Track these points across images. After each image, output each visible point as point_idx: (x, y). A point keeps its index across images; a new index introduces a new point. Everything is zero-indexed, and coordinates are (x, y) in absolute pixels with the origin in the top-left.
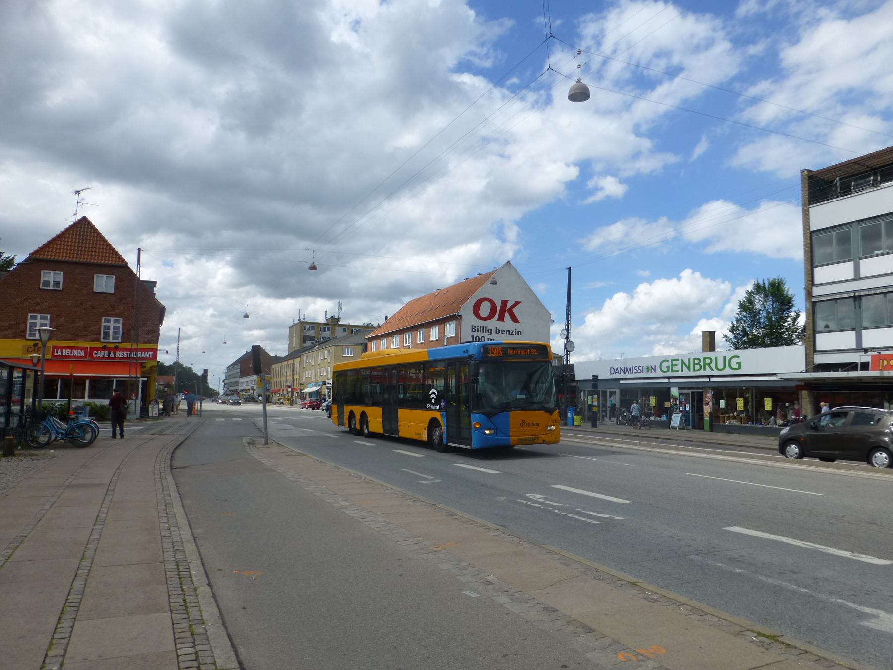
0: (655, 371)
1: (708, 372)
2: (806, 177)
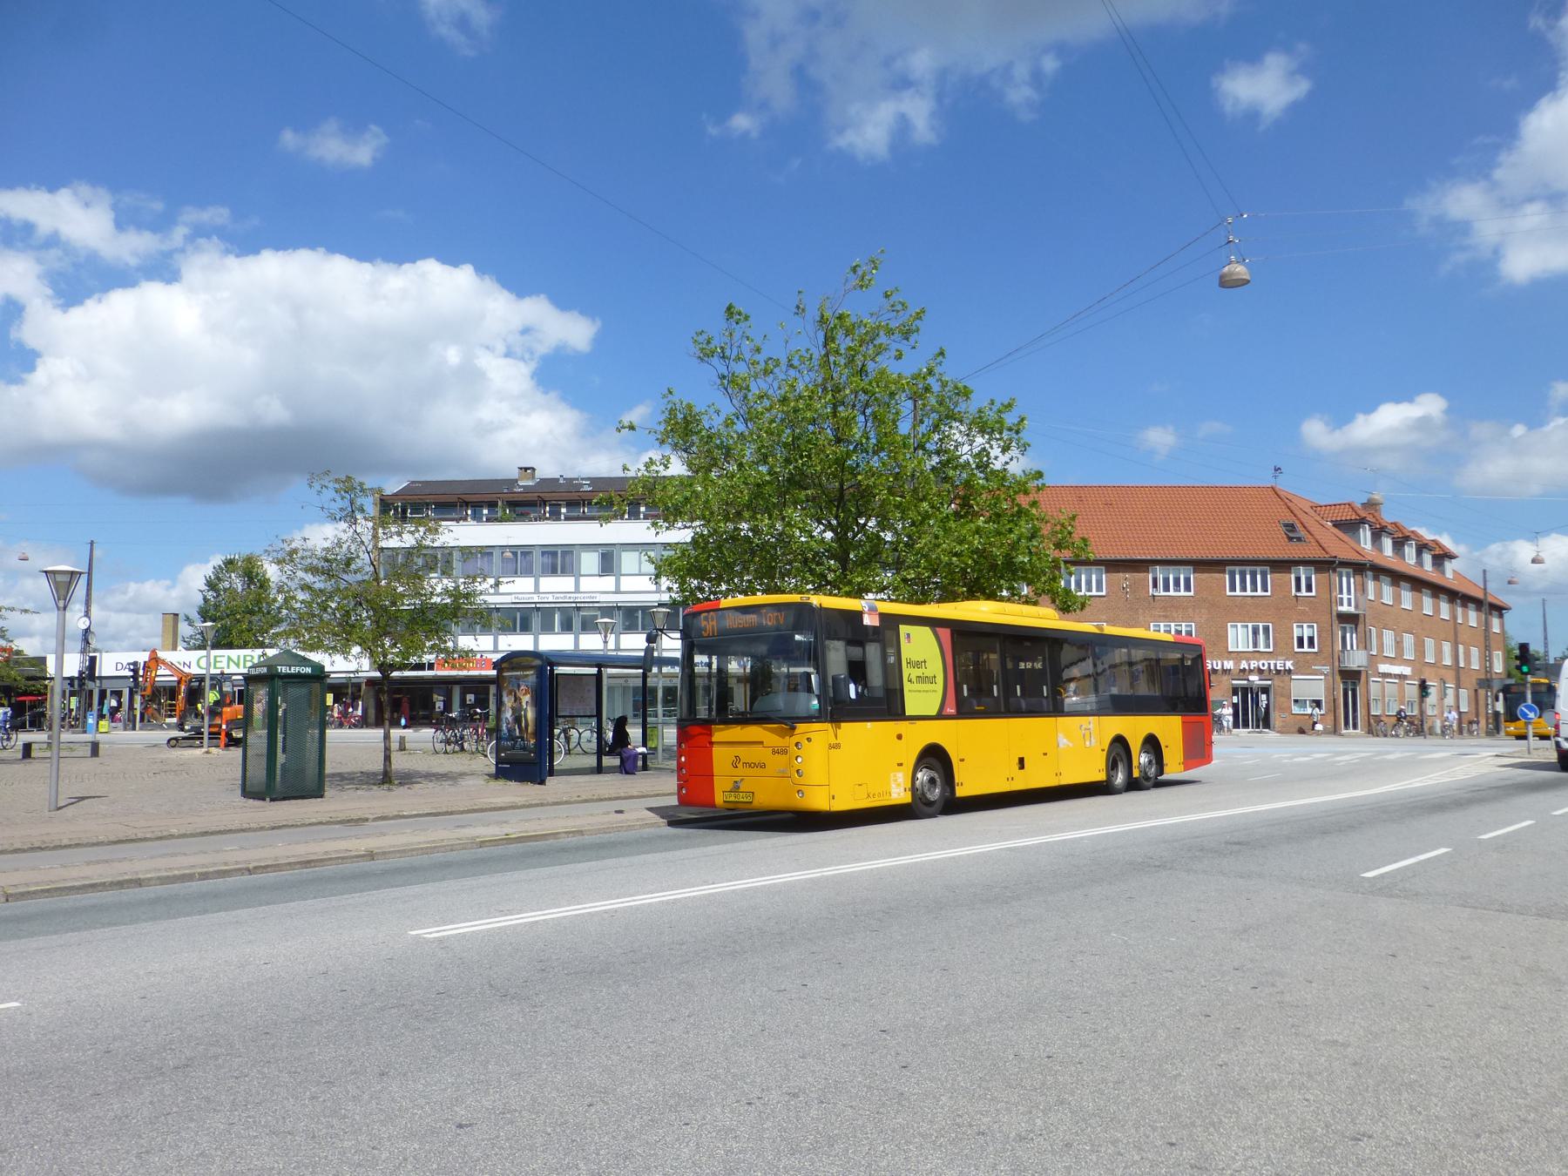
0: (189, 667)
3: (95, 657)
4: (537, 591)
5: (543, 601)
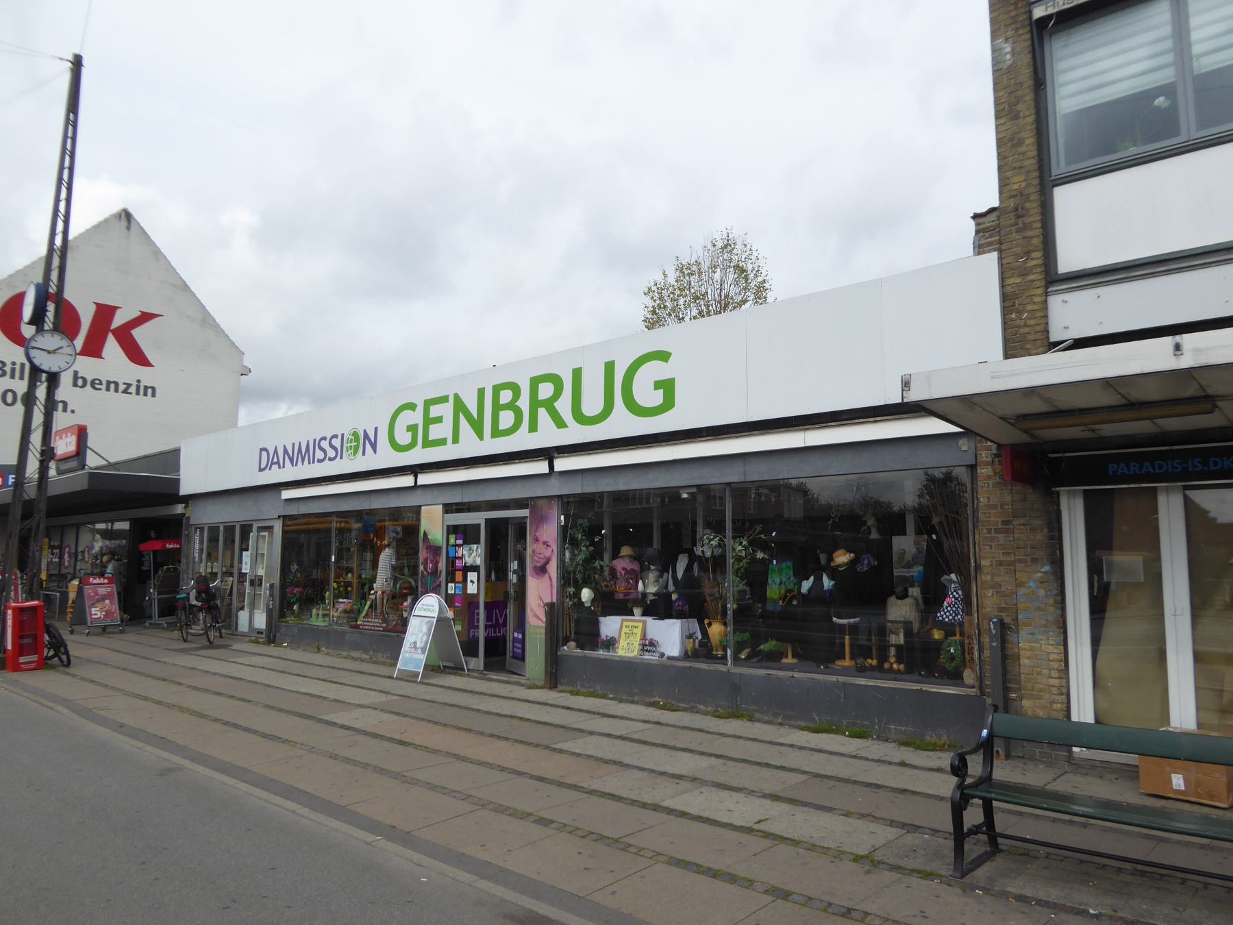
1: (548, 436)
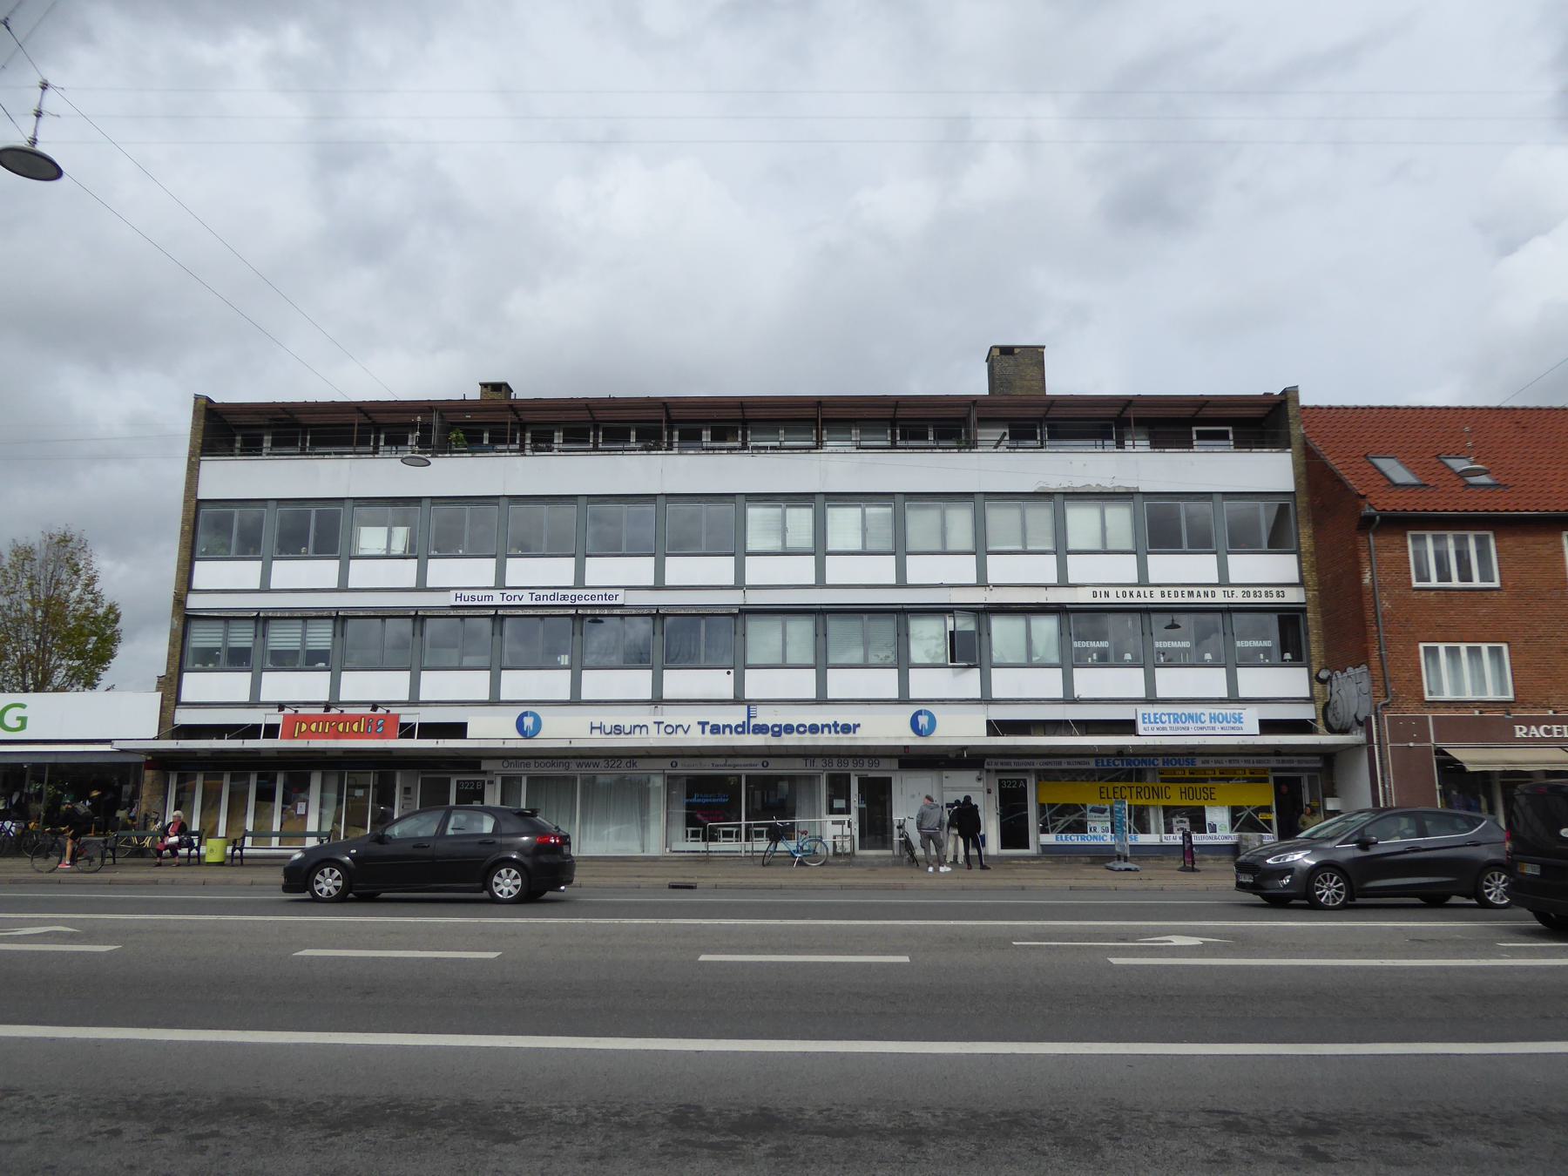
2: (203, 409)
3: (1227, 438)
4: (500, 584)
5: (512, 603)
